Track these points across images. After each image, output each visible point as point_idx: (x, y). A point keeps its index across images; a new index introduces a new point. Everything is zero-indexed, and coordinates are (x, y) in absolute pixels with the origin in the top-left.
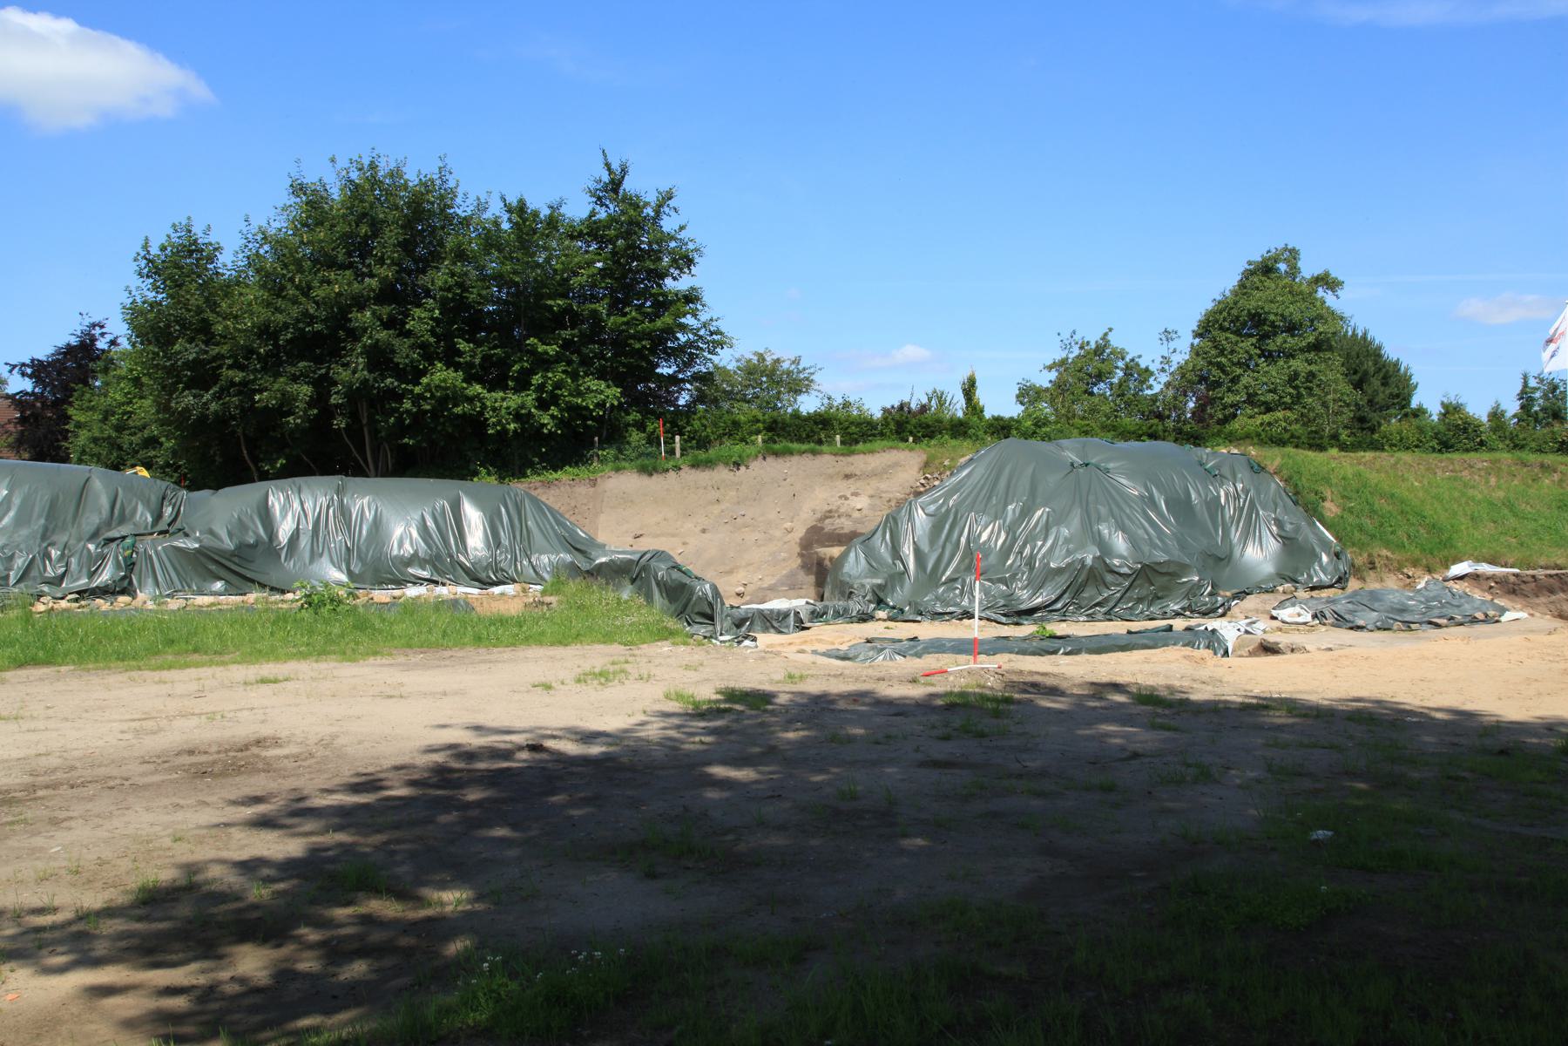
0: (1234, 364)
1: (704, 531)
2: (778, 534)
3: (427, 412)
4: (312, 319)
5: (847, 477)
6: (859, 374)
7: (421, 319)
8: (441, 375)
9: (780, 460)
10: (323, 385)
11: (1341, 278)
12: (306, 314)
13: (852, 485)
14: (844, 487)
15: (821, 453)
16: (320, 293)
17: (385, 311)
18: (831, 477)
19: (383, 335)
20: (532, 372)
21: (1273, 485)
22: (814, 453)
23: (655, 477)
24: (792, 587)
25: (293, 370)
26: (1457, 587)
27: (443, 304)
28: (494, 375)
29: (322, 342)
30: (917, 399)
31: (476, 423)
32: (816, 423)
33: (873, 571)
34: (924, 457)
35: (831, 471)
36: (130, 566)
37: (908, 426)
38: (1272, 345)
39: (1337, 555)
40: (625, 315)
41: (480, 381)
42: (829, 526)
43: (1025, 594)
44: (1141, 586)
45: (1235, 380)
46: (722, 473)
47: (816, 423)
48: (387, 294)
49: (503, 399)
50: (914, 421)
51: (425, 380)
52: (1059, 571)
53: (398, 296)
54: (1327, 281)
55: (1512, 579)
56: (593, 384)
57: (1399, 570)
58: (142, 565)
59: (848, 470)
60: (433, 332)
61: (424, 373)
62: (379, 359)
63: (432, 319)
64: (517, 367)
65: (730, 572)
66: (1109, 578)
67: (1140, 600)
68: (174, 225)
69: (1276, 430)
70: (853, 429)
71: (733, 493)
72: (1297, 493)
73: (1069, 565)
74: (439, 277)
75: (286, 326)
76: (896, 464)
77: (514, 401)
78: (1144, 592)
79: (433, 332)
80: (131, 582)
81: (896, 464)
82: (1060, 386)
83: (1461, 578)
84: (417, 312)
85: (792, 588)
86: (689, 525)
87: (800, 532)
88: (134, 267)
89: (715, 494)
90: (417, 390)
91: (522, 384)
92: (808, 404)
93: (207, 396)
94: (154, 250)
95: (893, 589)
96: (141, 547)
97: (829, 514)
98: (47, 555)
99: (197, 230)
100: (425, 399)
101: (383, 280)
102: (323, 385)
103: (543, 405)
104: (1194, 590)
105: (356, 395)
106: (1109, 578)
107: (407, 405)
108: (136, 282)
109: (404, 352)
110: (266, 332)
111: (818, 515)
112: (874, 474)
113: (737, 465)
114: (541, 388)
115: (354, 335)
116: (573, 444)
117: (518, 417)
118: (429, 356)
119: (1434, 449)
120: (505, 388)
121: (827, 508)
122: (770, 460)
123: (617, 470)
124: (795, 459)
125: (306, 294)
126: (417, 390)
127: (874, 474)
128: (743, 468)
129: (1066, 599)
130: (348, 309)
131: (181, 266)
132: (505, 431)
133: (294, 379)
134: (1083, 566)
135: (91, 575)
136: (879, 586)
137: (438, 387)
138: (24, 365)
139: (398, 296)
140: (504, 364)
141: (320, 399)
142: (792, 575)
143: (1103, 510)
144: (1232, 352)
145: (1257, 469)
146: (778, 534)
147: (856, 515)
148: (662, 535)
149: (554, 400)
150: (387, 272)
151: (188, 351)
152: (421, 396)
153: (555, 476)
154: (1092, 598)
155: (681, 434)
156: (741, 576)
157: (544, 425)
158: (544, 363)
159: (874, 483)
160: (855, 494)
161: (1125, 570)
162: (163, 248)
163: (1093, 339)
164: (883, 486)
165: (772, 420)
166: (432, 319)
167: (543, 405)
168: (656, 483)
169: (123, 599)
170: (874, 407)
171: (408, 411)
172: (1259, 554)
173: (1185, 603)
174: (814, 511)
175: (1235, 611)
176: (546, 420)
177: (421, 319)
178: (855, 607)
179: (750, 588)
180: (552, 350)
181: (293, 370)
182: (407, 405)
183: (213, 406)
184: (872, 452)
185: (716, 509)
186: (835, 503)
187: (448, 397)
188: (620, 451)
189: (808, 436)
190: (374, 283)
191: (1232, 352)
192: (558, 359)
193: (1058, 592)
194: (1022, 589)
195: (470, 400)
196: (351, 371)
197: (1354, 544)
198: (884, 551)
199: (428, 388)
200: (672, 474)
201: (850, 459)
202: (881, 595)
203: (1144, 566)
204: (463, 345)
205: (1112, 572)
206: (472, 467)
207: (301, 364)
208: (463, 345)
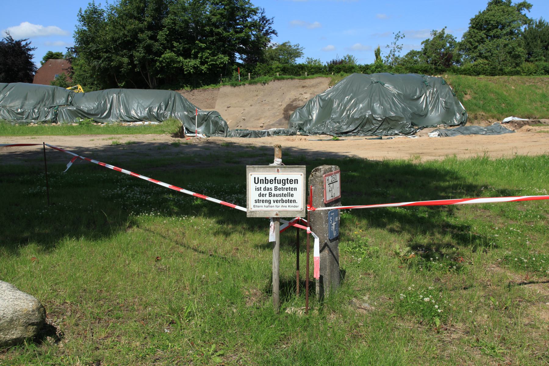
0: (476, 42)
1: (251, 106)
2: (276, 106)
3: (164, 66)
4: (126, 36)
5: (303, 87)
6: (317, 49)
7: (162, 35)
8: (168, 54)
9: (280, 81)
10: (131, 57)
11: (532, 4)
12: (124, 34)
13: (305, 90)
14: (301, 90)
15: (294, 79)
16: (128, 28)
17: (150, 33)
18: (297, 87)
19: (149, 41)
20: (198, 52)
21: (447, 89)
22: (292, 79)
23: (236, 88)
24: (280, 124)
25: (122, 53)
26: (505, 125)
27: (169, 29)
28: (186, 54)
29: (129, 44)
30: (341, 58)
31: (181, 70)
32: (299, 68)
33: (301, 119)
34: (330, 80)
35: (297, 85)
36: (56, 115)
37: (339, 68)
38: (492, 34)
39: (463, 114)
40: (229, 32)
41: (182, 55)
42: (294, 104)
43: (345, 127)
44: (385, 124)
45: (476, 48)
46: (259, 86)
47: (299, 68)
48: (150, 27)
49: (189, 62)
50: (335, 67)
51: (163, 56)
52: (357, 119)
53: (155, 27)
54: (480, 12)
55: (522, 123)
56: (221, 56)
57: (487, 120)
58: (59, 115)
59: (304, 85)
60: (166, 39)
61: (163, 53)
62: (148, 49)
63: (166, 35)
64: (193, 51)
65: (259, 119)
66: (374, 122)
67: (384, 129)
68: (89, 4)
69: (479, 68)
70: (313, 70)
71: (262, 93)
72: (456, 92)
73: (360, 117)
74: (166, 21)
75: (119, 39)
76: (321, 83)
77: (192, 62)
78: (386, 127)
79: (166, 39)
80: (56, 119)
81: (321, 83)
82: (425, 51)
83: (508, 122)
84: (160, 33)
85: (280, 124)
86: (246, 104)
87: (284, 106)
88: (77, 18)
89: (256, 93)
90: (161, 59)
91: (196, 57)
92: (299, 61)
93: (100, 62)
94: (83, 13)
95: (307, 125)
96: (59, 109)
97: (295, 100)
98: (34, 112)
99: (96, 4)
100: (163, 62)
101: (148, 22)
102: (131, 57)
103: (202, 63)
104: (403, 126)
105: (142, 61)
106: (374, 122)
107: (158, 64)
108: (78, 23)
109: (157, 46)
110: (114, 40)
111: (291, 100)
112: (313, 86)
113: (264, 83)
114: (201, 58)
115: (140, 41)
116: (214, 76)
117: (194, 68)
118: (165, 48)
119: (542, 74)
120: (190, 58)
121: (295, 98)
122: (276, 81)
123: (224, 85)
124: (285, 81)
125: (124, 28)
126: (161, 59)
127: (313, 86)
128: (266, 84)
129: (359, 128)
130: (137, 33)
131: (91, 18)
132: (190, 72)
133: (122, 56)
134: (365, 117)
135: (46, 117)
136: (301, 124)
137: (167, 58)
138: (72, 48)
139: (155, 27)
140: (189, 50)
141: (131, 63)
142: (280, 120)
143: (377, 98)
144: (475, 37)
145: (444, 83)
146: (276, 106)
147: (305, 100)
148: (237, 107)
149: (207, 62)
150: (149, 19)
151: (93, 47)
152: (162, 61)
153: (207, 87)
154: (367, 128)
155: (251, 72)
156: (262, 121)
157: (203, 70)
158: (202, 50)
159: (312, 89)
160: (305, 93)
161: (379, 119)
162: (86, 12)
163: (439, 30)
164: (315, 90)
165: (288, 67)
166: (166, 35)
167: (202, 63)
168: (236, 89)
169: (54, 124)
170: (325, 61)
171: (158, 66)
172: (434, 115)
173: (401, 130)
174: (290, 99)
175: (418, 133)
176: (203, 68)
177: (162, 35)
178: (292, 130)
179: (265, 125)
180: (203, 45)
181: (122, 53)
182: (158, 64)
183: (102, 65)
184: (313, 78)
185: (256, 98)
186: (298, 96)
187: (172, 61)
188: (230, 79)
189: (296, 73)
190: (146, 23)
191: (475, 37)
192: (206, 48)
193: (356, 126)
194: (344, 125)
195: (179, 62)
196: (139, 53)
197: (470, 110)
198: (306, 113)
199: (164, 58)
200: (242, 86)
201: (304, 81)
202: (302, 127)
203: (386, 118)
204: (175, 44)
205: (375, 119)
206: (181, 84)
207: (124, 51)
208: (175, 44)
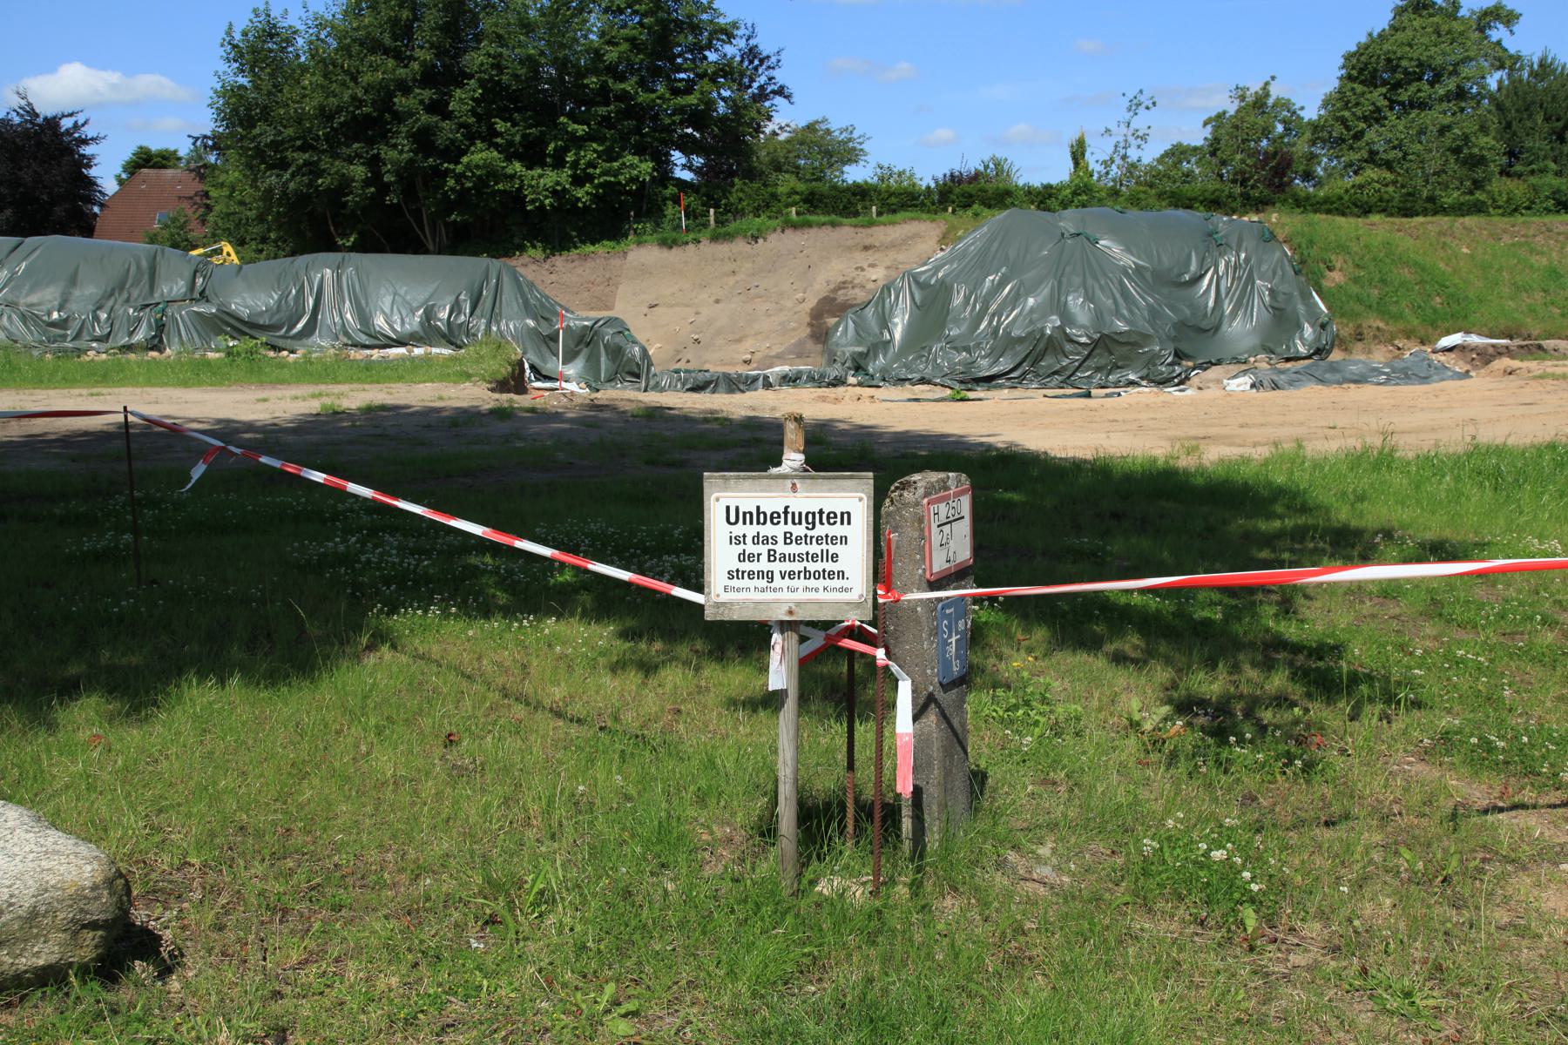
0: (1359, 119)
1: (717, 301)
2: (789, 304)
3: (470, 189)
4: (359, 102)
5: (866, 248)
6: (906, 141)
7: (461, 100)
8: (480, 155)
9: (798, 233)
10: (374, 163)
11: (1518, 11)
12: (354, 98)
13: (871, 257)
14: (861, 258)
15: (841, 225)
16: (366, 79)
17: (427, 94)
18: (849, 249)
19: (425, 118)
20: (565, 150)
21: (1278, 254)
22: (833, 225)
23: (675, 250)
24: (799, 355)
25: (348, 151)
26: (1441, 358)
27: (482, 83)
28: (532, 154)
29: (369, 125)
30: (973, 164)
31: (516, 199)
32: (854, 194)
33: (859, 339)
34: (944, 227)
35: (849, 243)
36: (160, 327)
37: (969, 194)
38: (1404, 96)
39: (1323, 326)
40: (654, 91)
41: (520, 158)
42: (841, 296)
43: (984, 363)
44: (1100, 355)
45: (1358, 136)
46: (740, 246)
47: (854, 194)
48: (429, 77)
49: (541, 176)
50: (957, 190)
51: (465, 159)
52: (1020, 340)
53: (443, 77)
54: (1370, 35)
55: (1491, 350)
56: (630, 159)
57: (1390, 341)
58: (170, 327)
59: (868, 242)
60: (473, 112)
61: (464, 153)
62: (424, 140)
63: (473, 99)
64: (551, 147)
65: (739, 341)
66: (1068, 347)
67: (1098, 369)
68: (255, 10)
69: (1368, 195)
70: (893, 200)
71: (749, 265)
72: (1303, 262)
73: (1029, 334)
74: (475, 59)
75: (339, 110)
76: (916, 236)
77: (550, 178)
78: (1103, 362)
79: (473, 112)
80: (161, 341)
81: (916, 236)
82: (1214, 146)
83: (1451, 349)
84: (458, 93)
85: (800, 354)
86: (704, 296)
87: (812, 302)
88: (221, 51)
89: (731, 266)
90: (459, 169)
91: (559, 163)
92: (854, 174)
93: (287, 176)
94: (238, 36)
95: (876, 357)
96: (169, 311)
97: (843, 285)
98: (96, 318)
99: (275, 13)
100: (467, 178)
101: (423, 63)
102: (374, 163)
103: (578, 181)
104: (1152, 360)
105: (407, 174)
106: (1068, 347)
107: (451, 182)
108: (223, 67)
109: (447, 131)
110: (325, 115)
111: (832, 286)
112: (893, 246)
113: (755, 238)
114: (575, 165)
115: (399, 118)
116: (610, 217)
117: (554, 193)
118: (471, 138)
119: (1548, 211)
120: (543, 165)
121: (841, 279)
122: (789, 232)
123: (639, 243)
124: (814, 231)
125: (354, 79)
126: (459, 169)
127: (893, 246)
128: (761, 241)
129: (1025, 366)
130: (391, 95)
131: (261, 50)
132: (542, 206)
133: (350, 160)
134: (1043, 334)
135: (131, 334)
136: (861, 354)
137: (477, 167)
138: (205, 137)
139: (443, 77)
140: (541, 142)
141: (375, 179)
142: (800, 343)
143: (1077, 280)
144: (1357, 104)
145: (1269, 237)
146: (789, 304)
147: (870, 286)
148: (677, 305)
149: (590, 178)
150: (425, 55)
151: (265, 133)
152: (463, 175)
153: (592, 248)
154: (1049, 366)
155: (716, 207)
156: (749, 344)
157: (579, 199)
158: (578, 142)
159: (892, 254)
160: (872, 266)
161: (1083, 340)
162: (245, 34)
163: (1255, 87)
164: (901, 257)
165: (823, 190)
166: (473, 99)
167: (578, 181)
168: (675, 255)
169: (155, 354)
170: (928, 174)
171: (452, 189)
172: (1240, 329)
173: (1145, 372)
174: (828, 283)
175: (1195, 381)
176: (580, 193)
177: (461, 100)
178: (833, 372)
179: (758, 356)
180: (581, 129)
181: (348, 151)
182: (451, 182)
183: (292, 185)
184: (893, 223)
185: (732, 280)
186: (851, 274)
187: (493, 174)
188: (658, 225)
189: (845, 208)
190: (416, 66)
191: (1357, 104)
192: (589, 137)
193: (1018, 360)
194: (984, 357)
195: (512, 177)
196: (397, 152)
197: (1342, 315)
198: (873, 324)
199: (468, 166)
200: (691, 247)
201: (869, 231)
202: (862, 363)
203: (1103, 336)
204: (501, 126)
205: (1071, 341)
206: (517, 241)
207: (356, 145)
208: (501, 126)
